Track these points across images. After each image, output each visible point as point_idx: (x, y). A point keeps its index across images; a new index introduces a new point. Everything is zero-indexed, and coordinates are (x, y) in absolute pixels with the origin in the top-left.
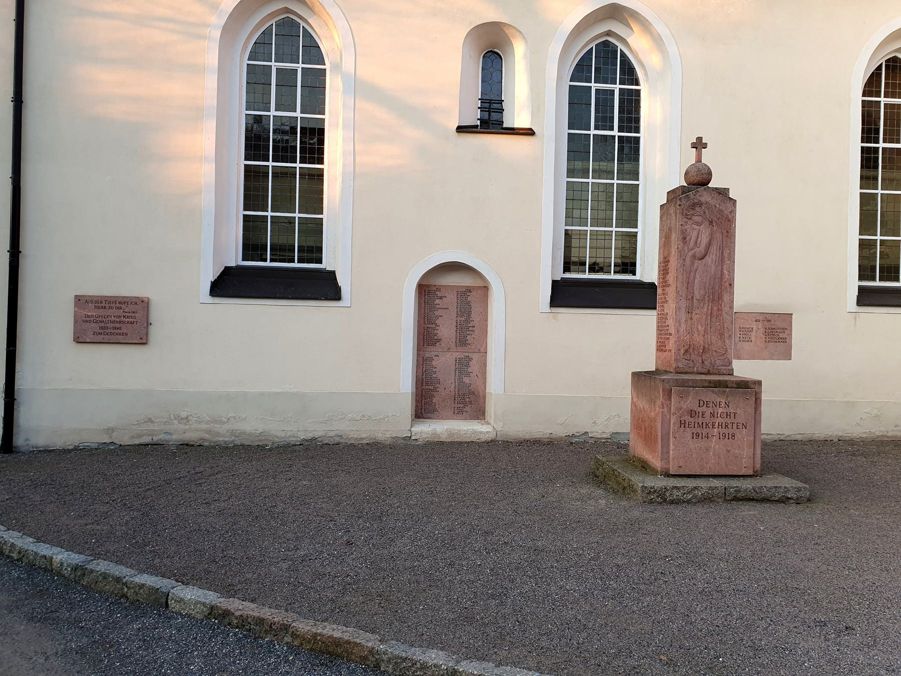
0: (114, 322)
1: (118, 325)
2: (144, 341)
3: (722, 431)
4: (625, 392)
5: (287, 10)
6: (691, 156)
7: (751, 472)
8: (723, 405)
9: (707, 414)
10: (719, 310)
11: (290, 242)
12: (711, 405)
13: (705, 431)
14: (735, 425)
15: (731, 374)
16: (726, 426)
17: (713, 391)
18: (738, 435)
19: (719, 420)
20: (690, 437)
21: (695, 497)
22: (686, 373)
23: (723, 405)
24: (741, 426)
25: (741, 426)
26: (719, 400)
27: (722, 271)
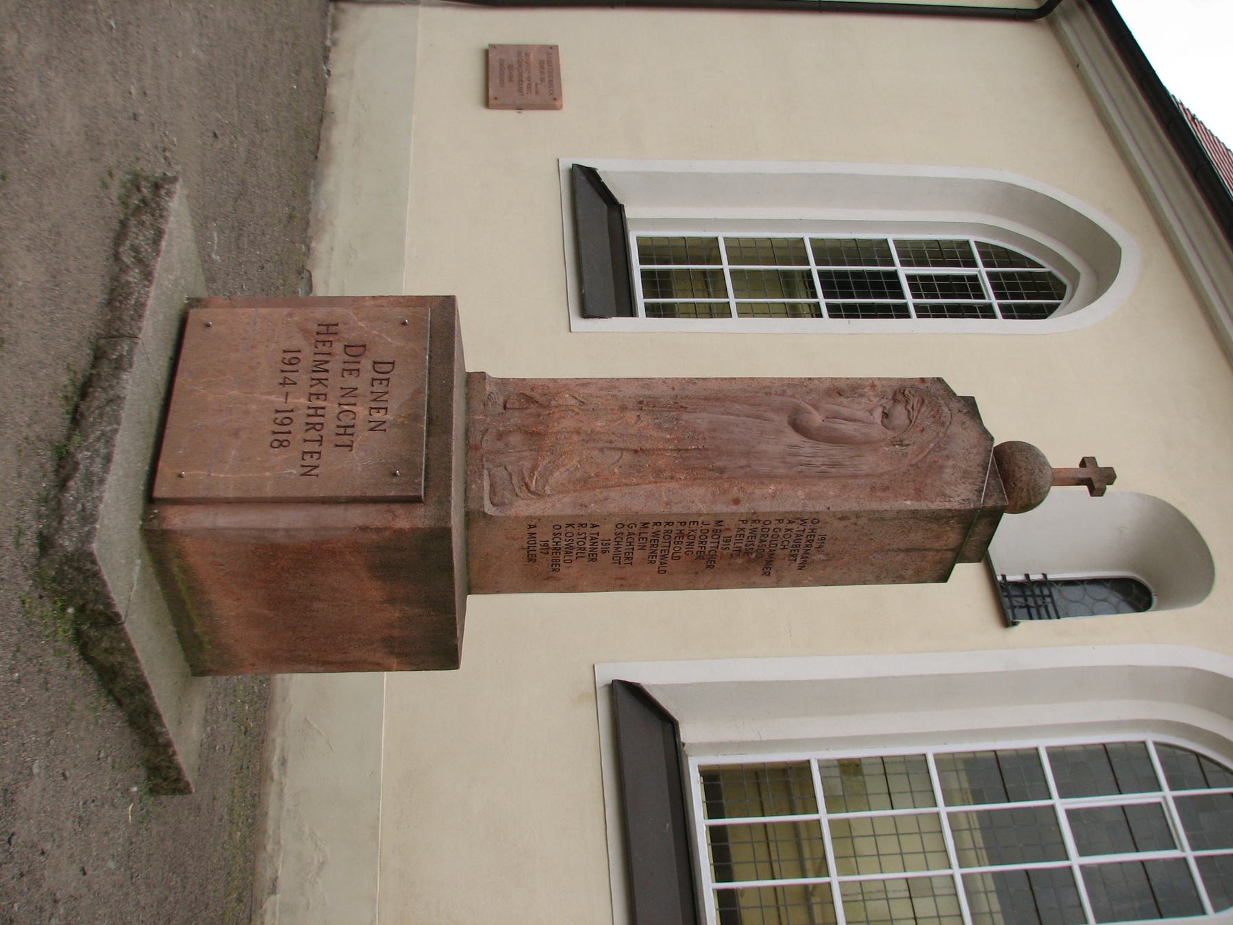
0: (520, 75)
1: (516, 78)
2: (492, 102)
3: (300, 420)
4: (418, 281)
5: (1075, 276)
6: (1062, 457)
7: (161, 491)
8: (378, 416)
9: (351, 381)
10: (658, 472)
11: (737, 869)
12: (378, 388)
13: (303, 378)
14: (315, 447)
15: (470, 590)
16: (312, 426)
17: (418, 392)
18: (279, 456)
19: (332, 408)
20: (287, 345)
21: (124, 269)
22: (468, 399)
23: (378, 416)
24: (309, 461)
25: (309, 461)
26: (393, 405)
27: (772, 477)
